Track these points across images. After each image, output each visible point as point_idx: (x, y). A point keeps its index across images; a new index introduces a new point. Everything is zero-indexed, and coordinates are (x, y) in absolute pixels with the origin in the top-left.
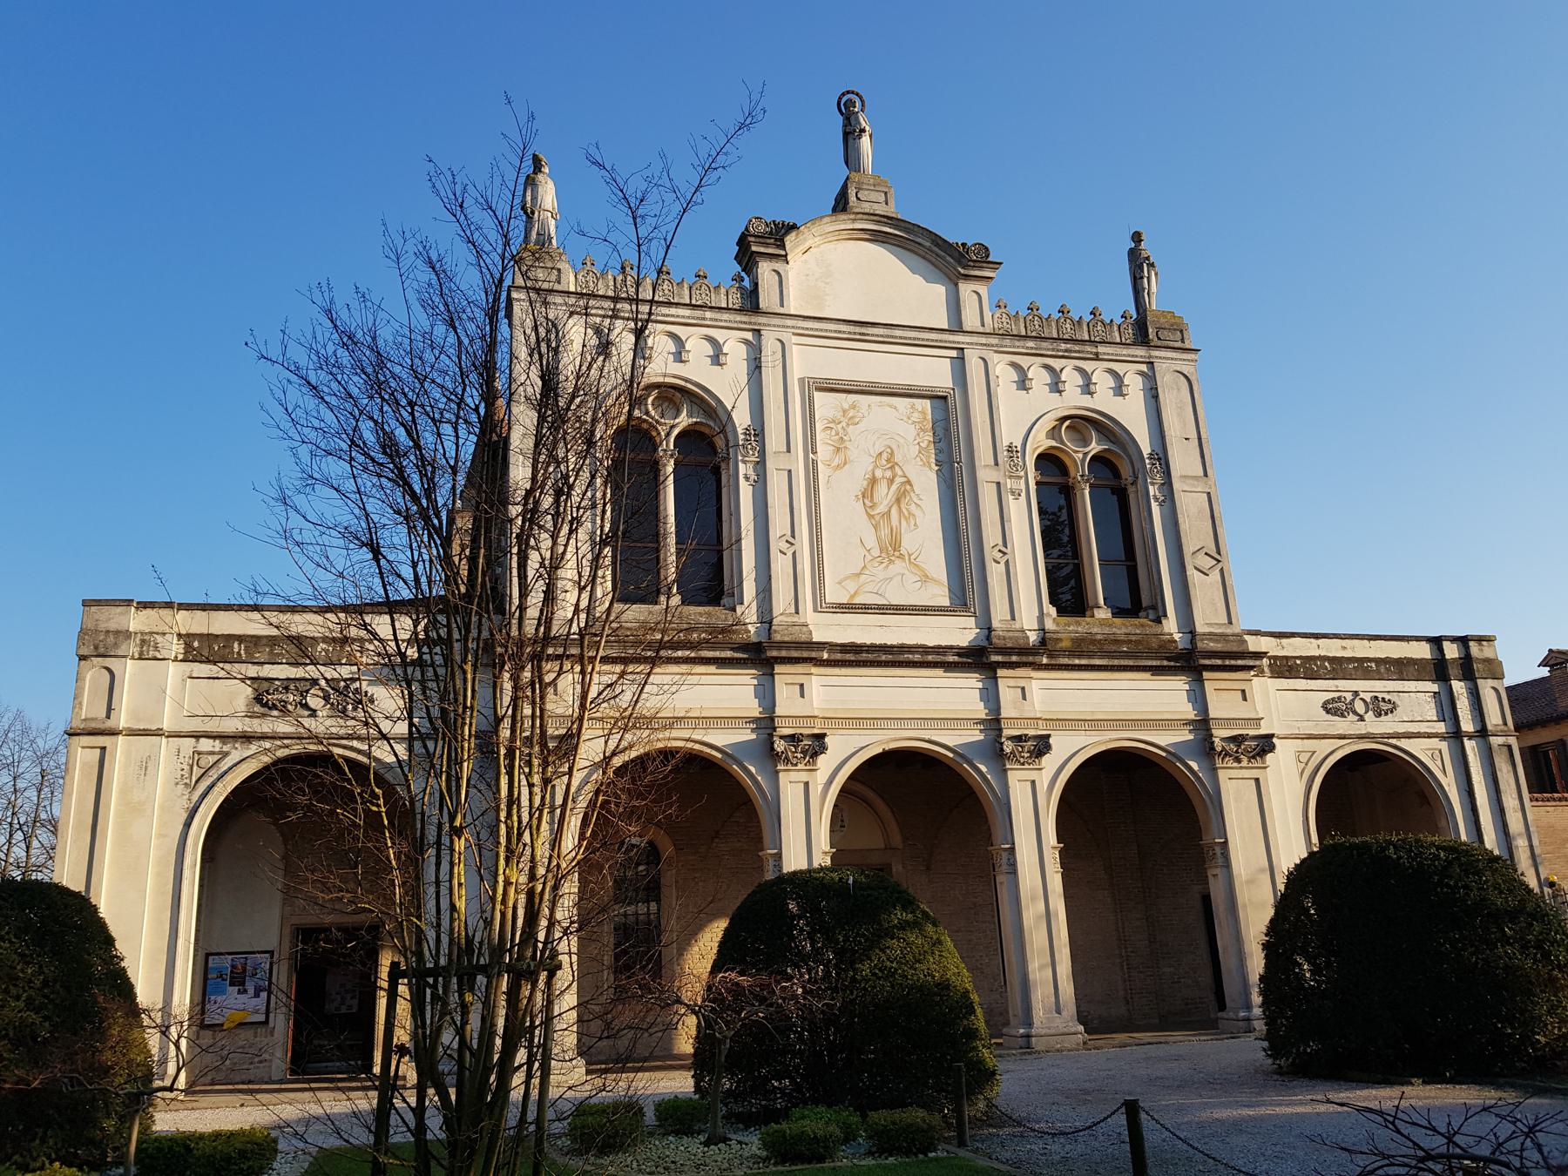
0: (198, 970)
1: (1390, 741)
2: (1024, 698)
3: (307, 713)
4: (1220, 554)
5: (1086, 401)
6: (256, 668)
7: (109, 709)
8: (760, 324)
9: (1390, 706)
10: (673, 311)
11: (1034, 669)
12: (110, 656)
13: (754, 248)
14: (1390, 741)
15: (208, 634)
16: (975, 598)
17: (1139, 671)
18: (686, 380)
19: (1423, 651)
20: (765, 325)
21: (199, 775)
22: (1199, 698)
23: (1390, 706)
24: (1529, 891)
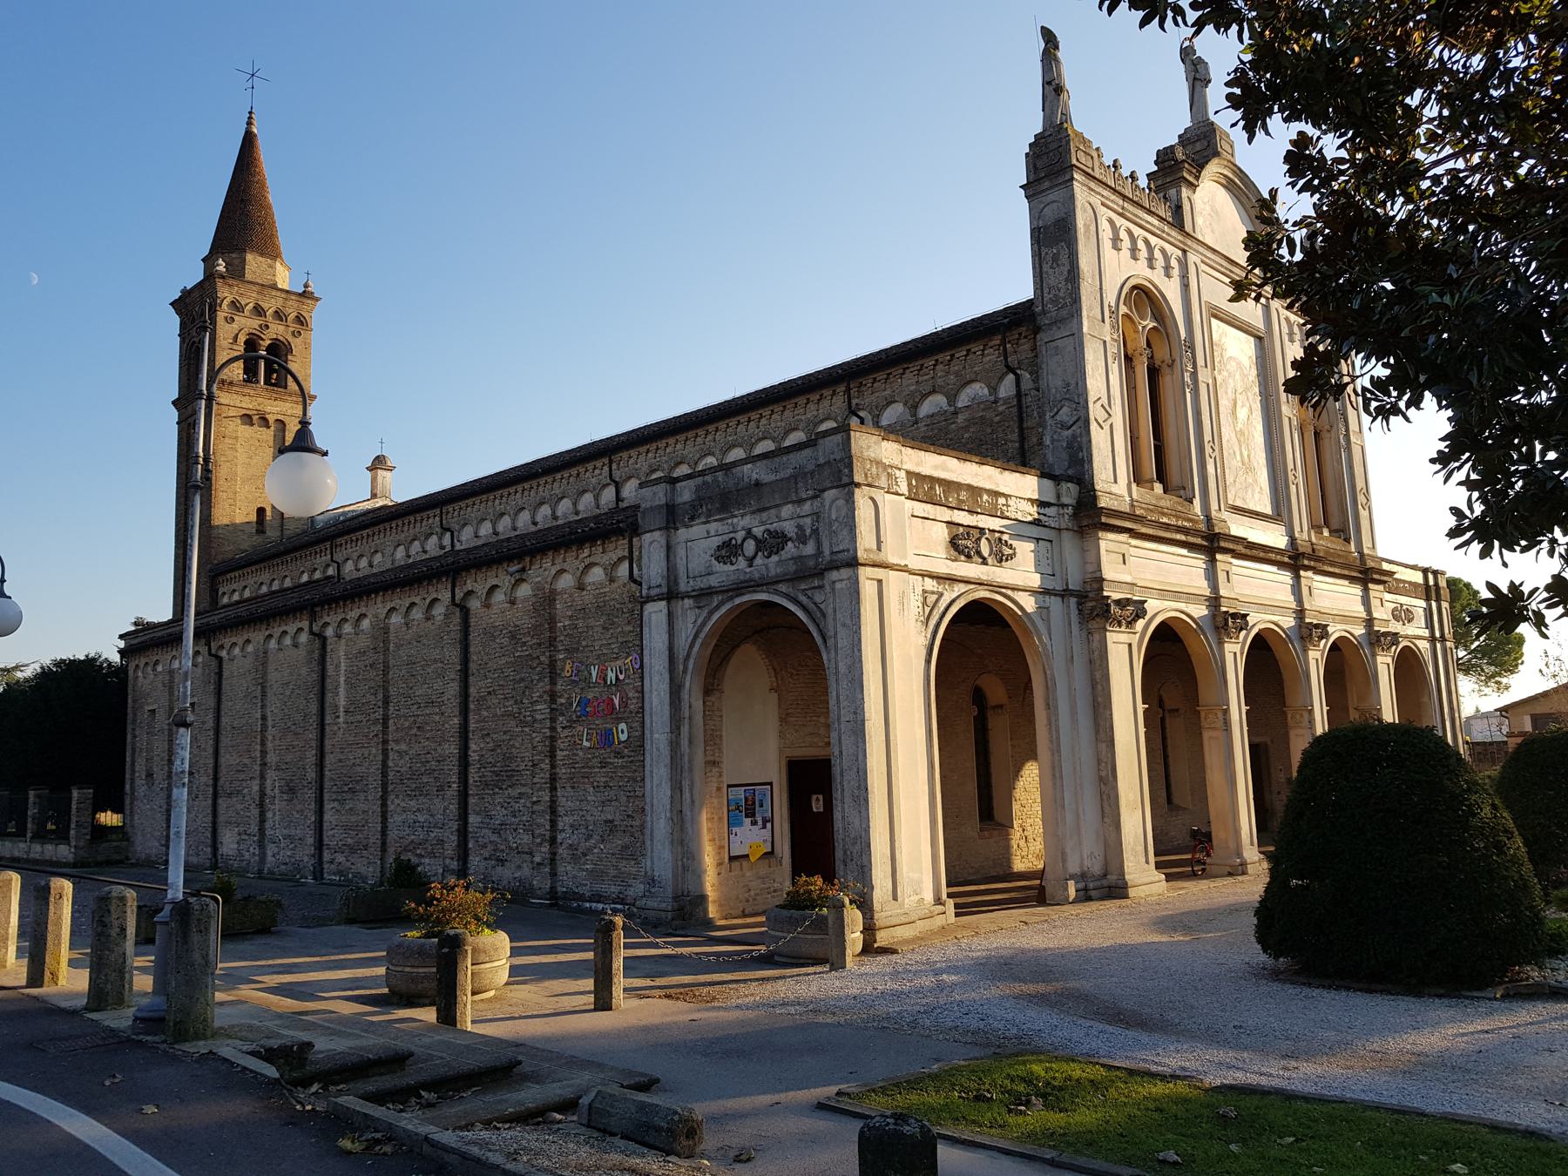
0: (850, 777)
1: (1003, 590)
2: (1228, 581)
3: (980, 560)
4: (1110, 407)
5: (1148, 273)
6: (949, 512)
7: (879, 542)
8: (1189, 247)
9: (1011, 552)
10: (1149, 218)
11: (1130, 537)
12: (875, 487)
13: (1185, 175)
14: (1009, 592)
15: (850, 457)
16: (1285, 514)
17: (1171, 544)
18: (1156, 288)
19: (1418, 577)
20: (1195, 250)
21: (928, 603)
22: (1211, 575)
23: (1011, 552)
24: (1448, 744)
